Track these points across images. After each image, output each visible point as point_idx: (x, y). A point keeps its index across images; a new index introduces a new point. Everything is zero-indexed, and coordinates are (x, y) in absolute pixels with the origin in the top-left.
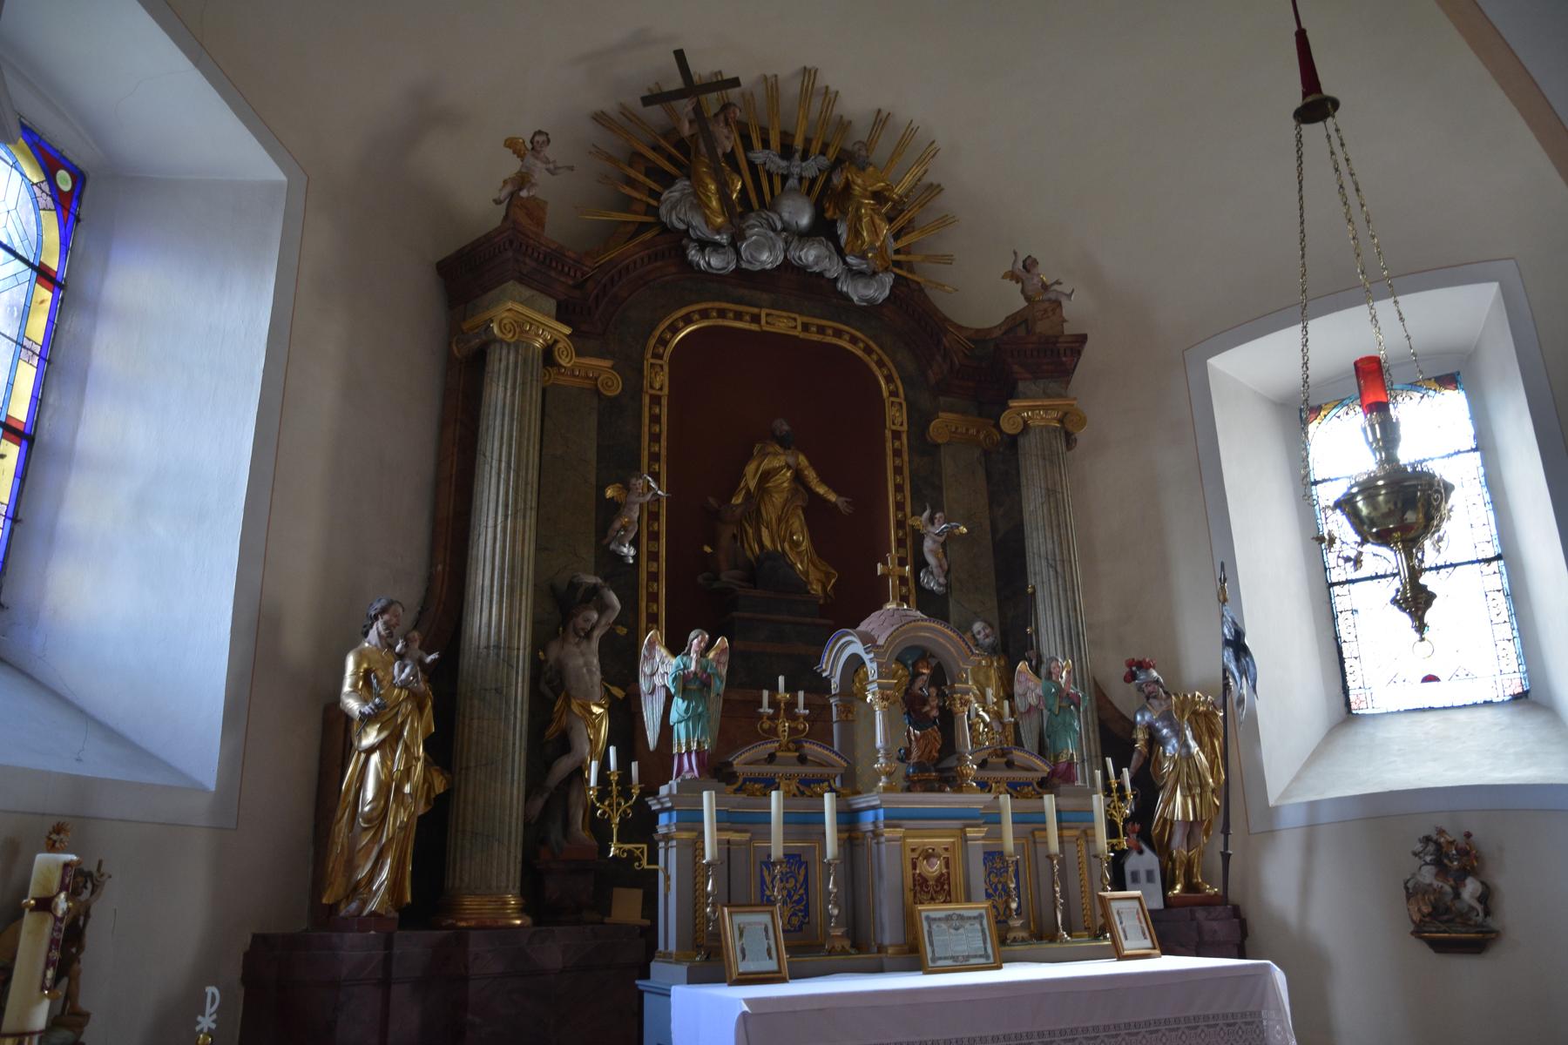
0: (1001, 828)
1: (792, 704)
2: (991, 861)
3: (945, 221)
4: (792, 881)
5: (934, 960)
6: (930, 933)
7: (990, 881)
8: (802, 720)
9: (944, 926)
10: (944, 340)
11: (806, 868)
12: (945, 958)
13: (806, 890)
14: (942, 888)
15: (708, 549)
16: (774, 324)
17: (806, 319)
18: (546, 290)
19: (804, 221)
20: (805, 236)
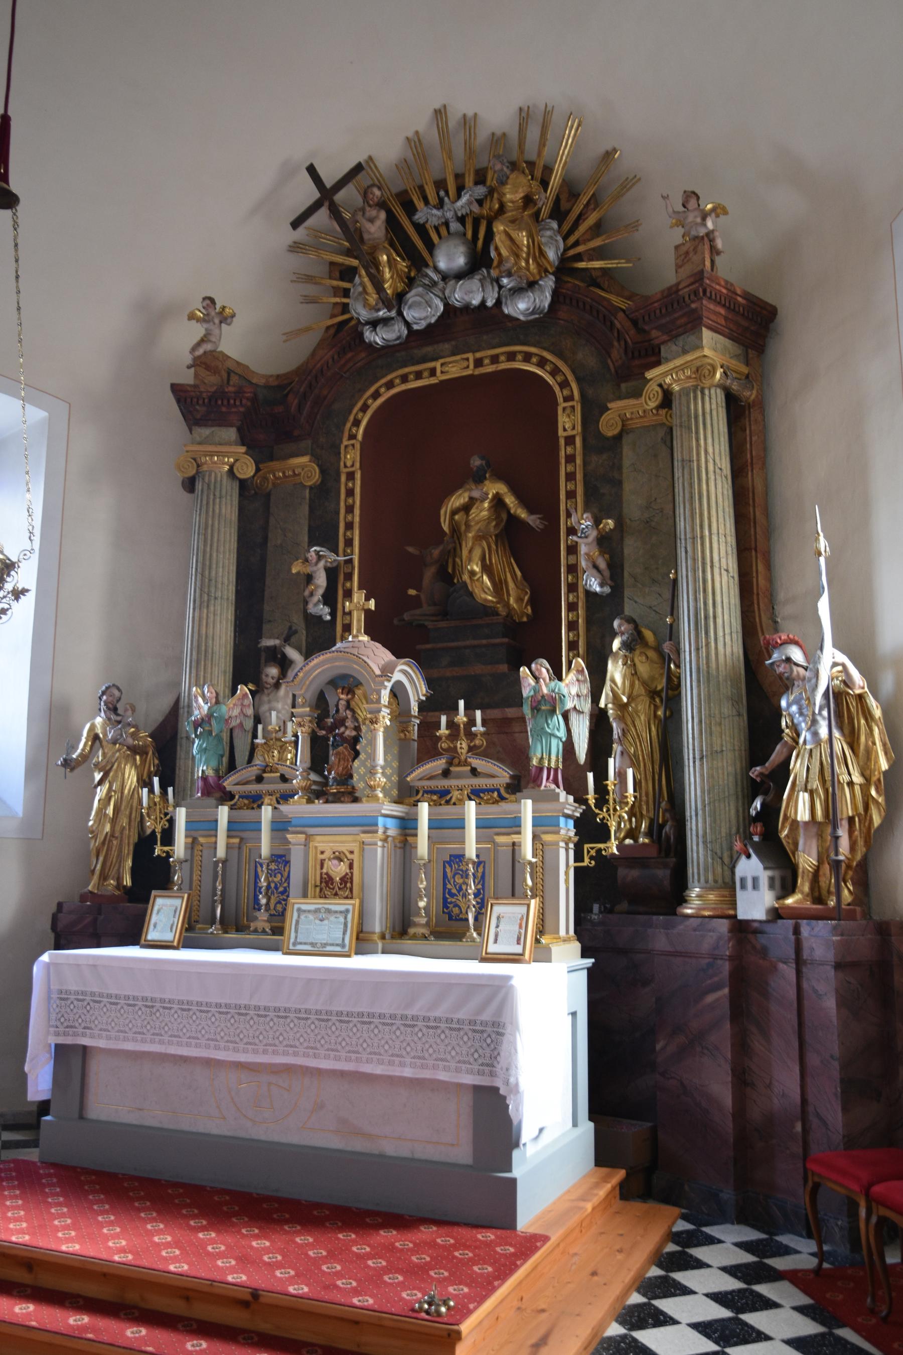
0: (464, 834)
1: (472, 722)
2: (457, 863)
3: (629, 183)
4: (279, 876)
5: (294, 944)
6: (297, 922)
7: (454, 881)
8: (479, 737)
9: (311, 917)
10: (616, 322)
11: (484, 867)
12: (305, 944)
13: (483, 885)
14: (345, 886)
15: (412, 592)
16: (447, 372)
17: (478, 355)
18: (222, 421)
19: (460, 261)
20: (460, 276)
